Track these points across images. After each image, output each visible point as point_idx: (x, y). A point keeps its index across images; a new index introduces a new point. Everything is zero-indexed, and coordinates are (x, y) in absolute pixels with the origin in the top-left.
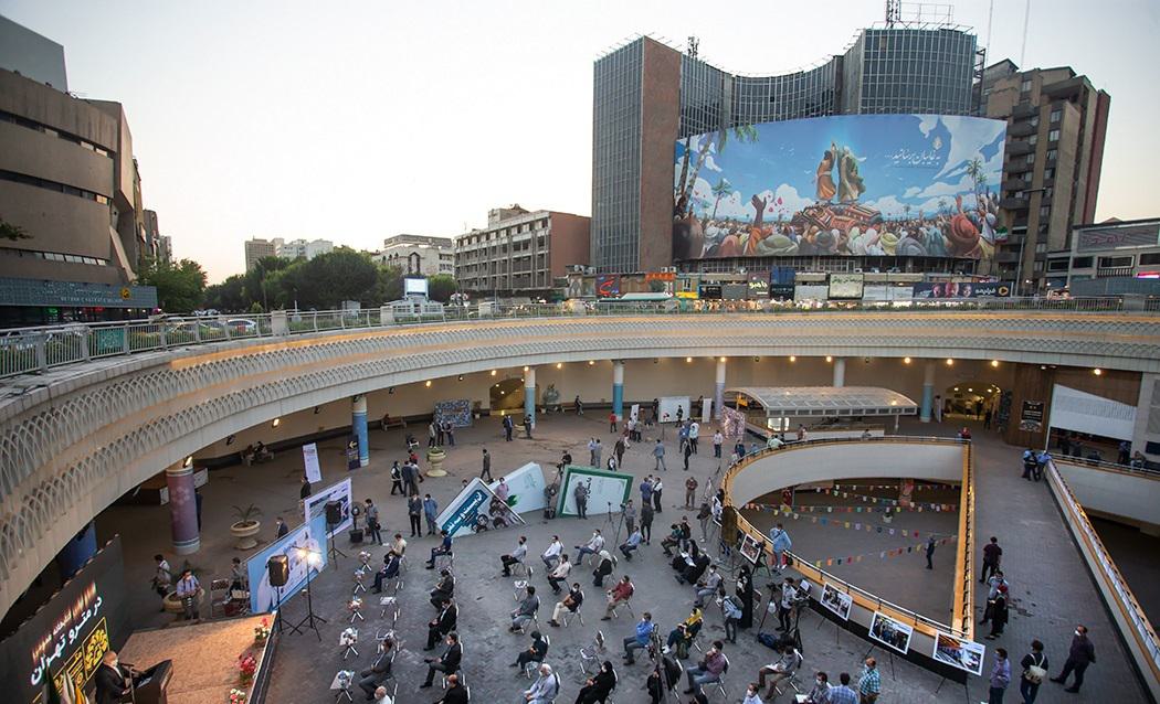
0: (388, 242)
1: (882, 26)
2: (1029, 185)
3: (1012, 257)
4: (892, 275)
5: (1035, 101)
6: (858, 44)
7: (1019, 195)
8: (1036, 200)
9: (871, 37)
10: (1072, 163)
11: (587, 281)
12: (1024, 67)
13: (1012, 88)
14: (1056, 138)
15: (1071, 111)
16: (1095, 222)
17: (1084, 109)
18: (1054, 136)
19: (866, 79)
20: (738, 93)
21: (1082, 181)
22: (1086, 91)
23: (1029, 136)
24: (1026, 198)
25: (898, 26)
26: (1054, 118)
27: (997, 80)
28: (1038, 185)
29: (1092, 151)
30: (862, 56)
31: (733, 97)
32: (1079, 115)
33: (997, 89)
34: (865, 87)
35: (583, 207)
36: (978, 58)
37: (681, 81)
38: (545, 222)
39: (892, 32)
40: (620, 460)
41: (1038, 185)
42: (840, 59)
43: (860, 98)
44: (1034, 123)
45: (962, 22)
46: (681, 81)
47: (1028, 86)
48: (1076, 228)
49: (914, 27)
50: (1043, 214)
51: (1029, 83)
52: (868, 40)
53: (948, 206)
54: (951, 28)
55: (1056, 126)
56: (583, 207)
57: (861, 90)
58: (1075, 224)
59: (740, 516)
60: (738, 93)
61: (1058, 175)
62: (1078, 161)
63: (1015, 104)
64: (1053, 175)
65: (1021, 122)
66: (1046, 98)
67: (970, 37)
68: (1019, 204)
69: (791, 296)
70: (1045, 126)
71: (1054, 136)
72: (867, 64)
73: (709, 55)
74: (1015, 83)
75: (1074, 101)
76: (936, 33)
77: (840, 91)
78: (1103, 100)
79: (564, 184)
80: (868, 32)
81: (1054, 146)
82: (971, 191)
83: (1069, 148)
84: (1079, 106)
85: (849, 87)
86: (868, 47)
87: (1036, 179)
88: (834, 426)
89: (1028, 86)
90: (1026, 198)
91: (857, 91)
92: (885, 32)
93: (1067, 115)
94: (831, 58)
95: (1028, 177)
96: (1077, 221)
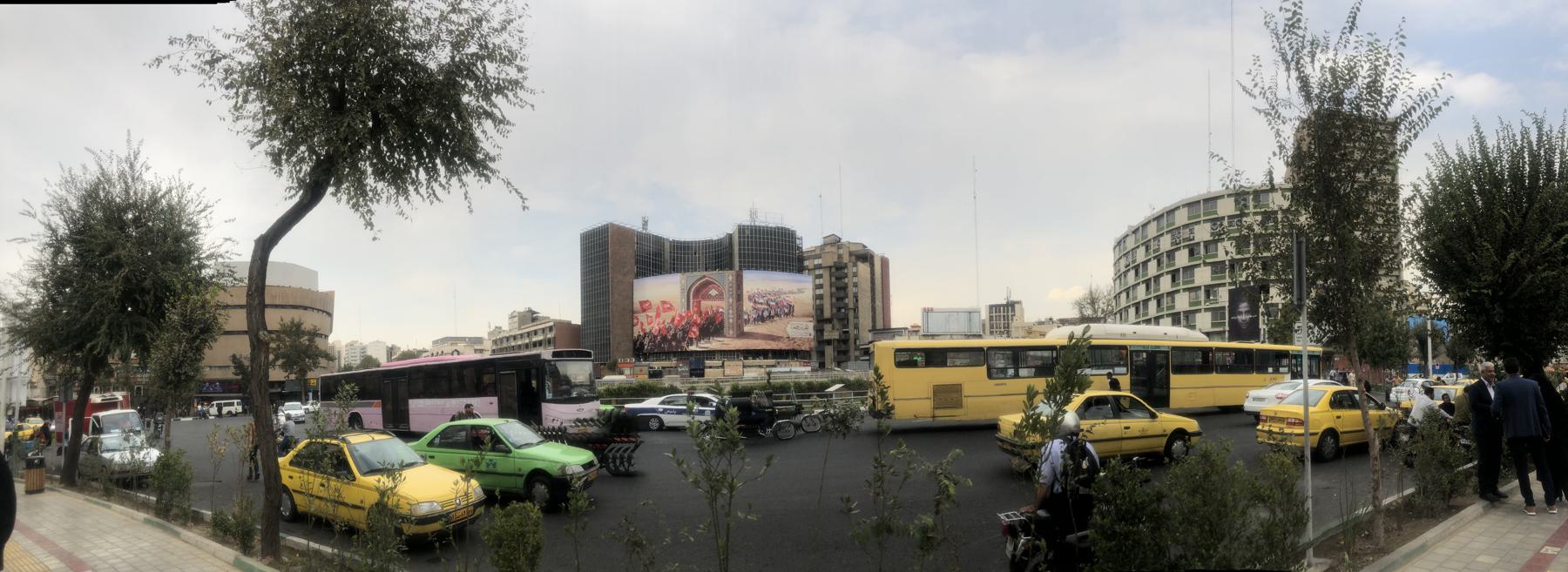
0: (435, 342)
3: (843, 347)
4: (758, 361)
8: (851, 315)
10: (869, 294)
11: (814, 355)
17: (872, 265)
21: (879, 303)
28: (851, 305)
35: (576, 319)
38: (551, 329)
42: (730, 236)
45: (789, 223)
53: (642, 317)
56: (576, 319)
59: (1085, 424)
69: (702, 375)
73: (655, 230)
78: (885, 263)
79: (564, 304)
82: (241, 307)
83: (866, 286)
87: (850, 301)
88: (437, 526)
96: (879, 325)
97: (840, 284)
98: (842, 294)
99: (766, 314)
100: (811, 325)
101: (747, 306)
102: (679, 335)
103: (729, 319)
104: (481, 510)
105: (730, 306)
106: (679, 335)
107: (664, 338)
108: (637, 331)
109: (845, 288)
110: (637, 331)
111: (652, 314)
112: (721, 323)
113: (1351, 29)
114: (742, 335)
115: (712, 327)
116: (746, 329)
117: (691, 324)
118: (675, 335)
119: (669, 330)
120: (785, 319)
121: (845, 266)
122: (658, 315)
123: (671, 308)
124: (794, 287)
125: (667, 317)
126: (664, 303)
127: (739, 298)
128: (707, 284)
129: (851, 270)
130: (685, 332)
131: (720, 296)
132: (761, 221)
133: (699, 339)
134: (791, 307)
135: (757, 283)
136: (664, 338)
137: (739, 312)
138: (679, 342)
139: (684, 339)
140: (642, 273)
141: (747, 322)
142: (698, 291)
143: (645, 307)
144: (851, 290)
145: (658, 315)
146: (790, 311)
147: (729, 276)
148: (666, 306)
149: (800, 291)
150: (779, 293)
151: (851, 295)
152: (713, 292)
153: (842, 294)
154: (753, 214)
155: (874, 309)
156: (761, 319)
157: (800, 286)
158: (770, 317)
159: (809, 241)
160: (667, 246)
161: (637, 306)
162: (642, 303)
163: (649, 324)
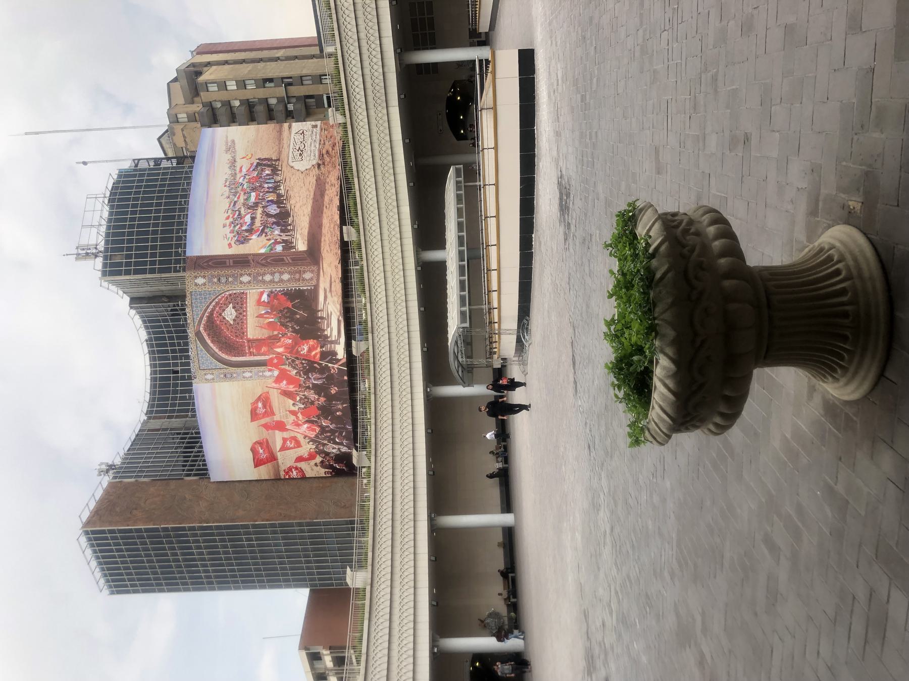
1: (99, 262)
2: (280, 100)
5: (197, 107)
6: (118, 284)
7: (291, 107)
8: (296, 91)
9: (111, 270)
12: (164, 122)
13: (182, 130)
14: (234, 83)
15: (208, 75)
16: (316, 35)
17: (209, 64)
18: (232, 85)
19: (152, 271)
20: (166, 412)
21: (280, 53)
22: (193, 65)
23: (231, 107)
24: (294, 100)
25: (101, 247)
26: (213, 88)
27: (175, 145)
28: (281, 91)
29: (245, 50)
30: (128, 277)
31: (169, 417)
32: (214, 67)
33: (183, 145)
34: (161, 271)
36: (165, 164)
37: (142, 480)
38: (314, 658)
39: (106, 250)
40: (882, 650)
41: (281, 91)
42: (135, 301)
43: (173, 274)
44: (219, 105)
46: (142, 480)
47: (183, 117)
48: (322, 50)
49: (103, 229)
50: (310, 82)
51: (179, 116)
52: (112, 273)
53: (286, 459)
54: (108, 194)
55: (223, 86)
57: (164, 275)
58: (318, 52)
60: (166, 412)
61: (270, 75)
62: (261, 60)
63: (199, 125)
64: (271, 80)
65: (213, 117)
66: (196, 99)
67: (119, 176)
68: (301, 106)
70: (224, 96)
71: (232, 85)
72: (137, 272)
74: (178, 128)
75: (199, 74)
76: (112, 207)
77: (167, 297)
78: (203, 50)
80: (104, 274)
81: (242, 84)
83: (244, 70)
84: (205, 69)
85: (163, 288)
86: (119, 273)
89: (183, 117)
90: (294, 100)
91: (165, 279)
92: (105, 258)
93: (212, 77)
94: (133, 312)
95: (273, 101)
96: (315, 50)
97: (241, 112)
98: (260, 109)
99: (273, 210)
100: (296, 126)
101: (257, 245)
102: (315, 379)
103: (284, 279)
104: (497, 364)
105: (257, 280)
106: (315, 379)
107: (326, 411)
108: (313, 469)
109: (249, 106)
110: (313, 469)
111: (278, 439)
112: (292, 295)
113: (599, 569)
114: (313, 255)
115: (299, 312)
116: (302, 246)
117: (294, 356)
118: (318, 389)
119: (306, 401)
120: (285, 173)
121: (210, 106)
122: (281, 426)
123: (265, 399)
124: (222, 160)
125: (283, 407)
126: (254, 415)
127: (242, 262)
128: (213, 326)
129: (213, 94)
130: (310, 367)
131: (239, 301)
132: (97, 237)
133: (323, 339)
134: (262, 164)
135: (210, 231)
136: (326, 411)
137: (270, 261)
138: (330, 379)
139: (324, 370)
140: (203, 472)
141: (288, 245)
142: (230, 347)
143: (263, 455)
144: (252, 92)
145: (281, 426)
146: (269, 166)
147: (197, 284)
148: (261, 410)
149: (231, 147)
150: (233, 186)
151: (261, 93)
152: (230, 314)
153: (260, 109)
154: (85, 254)
155: (288, 58)
156: (283, 219)
157: (220, 147)
158: (279, 202)
159: (144, 145)
160: (156, 424)
161: (263, 472)
162: (258, 463)
163: (299, 445)
